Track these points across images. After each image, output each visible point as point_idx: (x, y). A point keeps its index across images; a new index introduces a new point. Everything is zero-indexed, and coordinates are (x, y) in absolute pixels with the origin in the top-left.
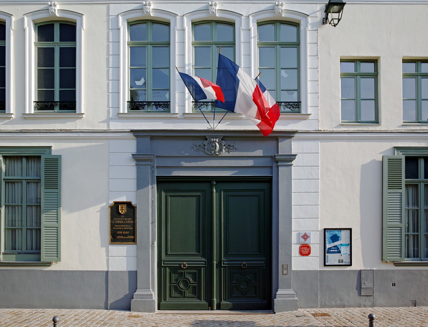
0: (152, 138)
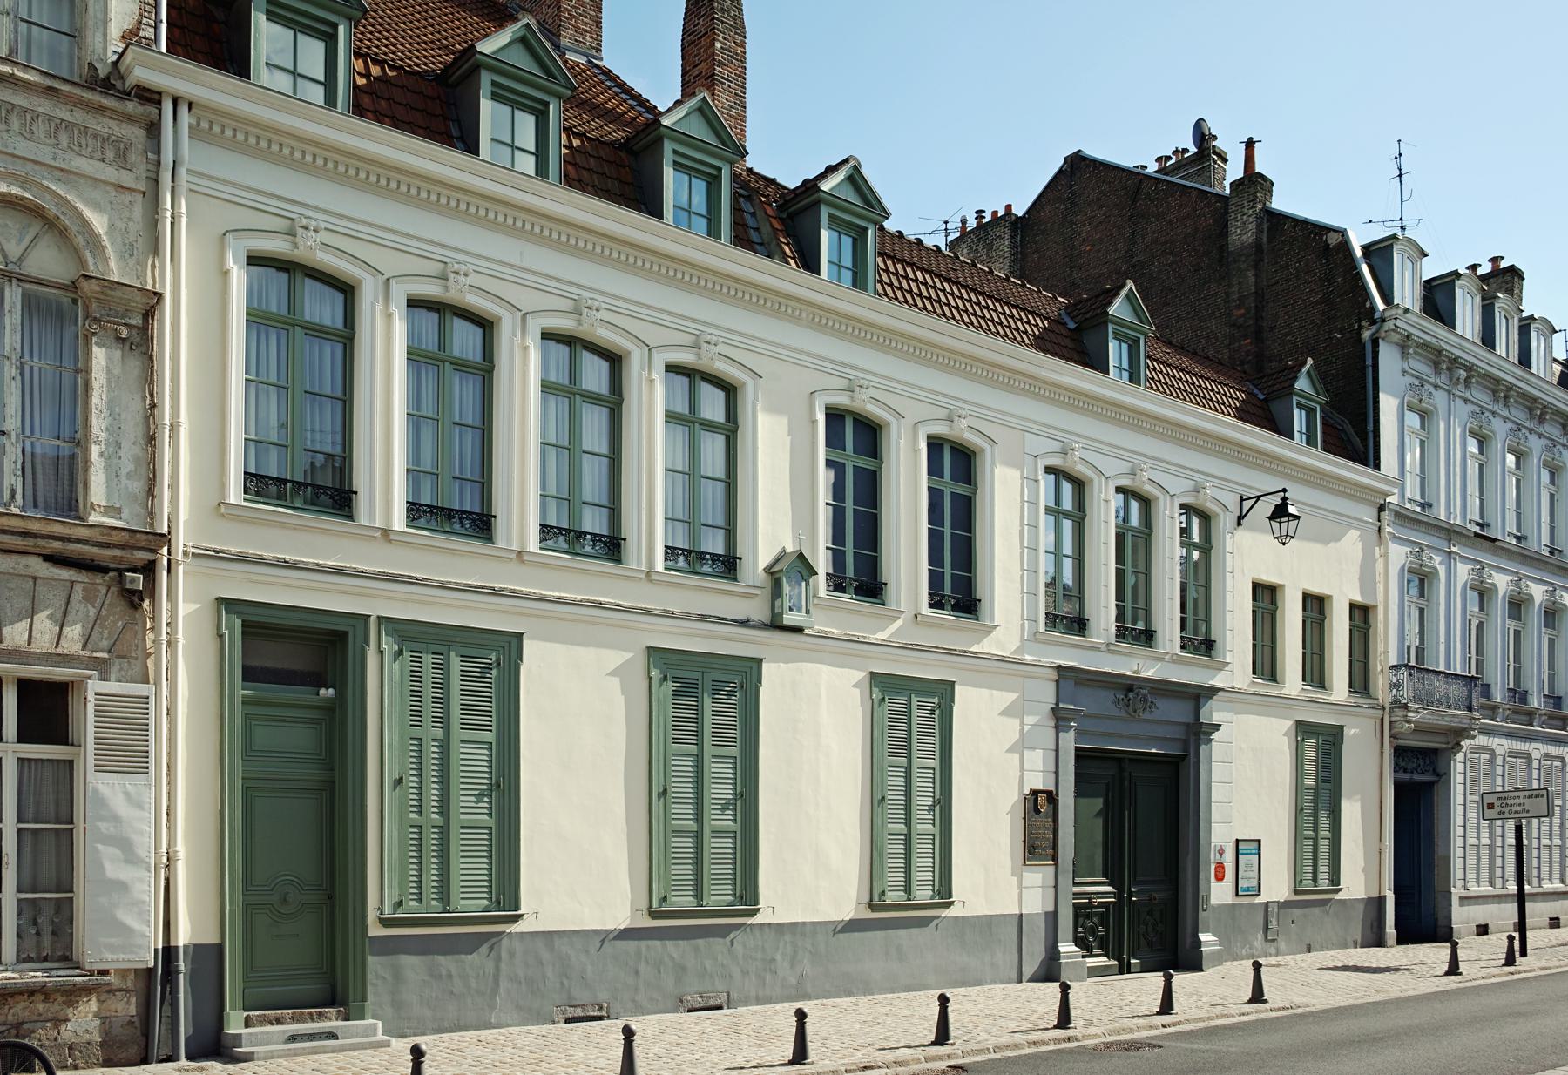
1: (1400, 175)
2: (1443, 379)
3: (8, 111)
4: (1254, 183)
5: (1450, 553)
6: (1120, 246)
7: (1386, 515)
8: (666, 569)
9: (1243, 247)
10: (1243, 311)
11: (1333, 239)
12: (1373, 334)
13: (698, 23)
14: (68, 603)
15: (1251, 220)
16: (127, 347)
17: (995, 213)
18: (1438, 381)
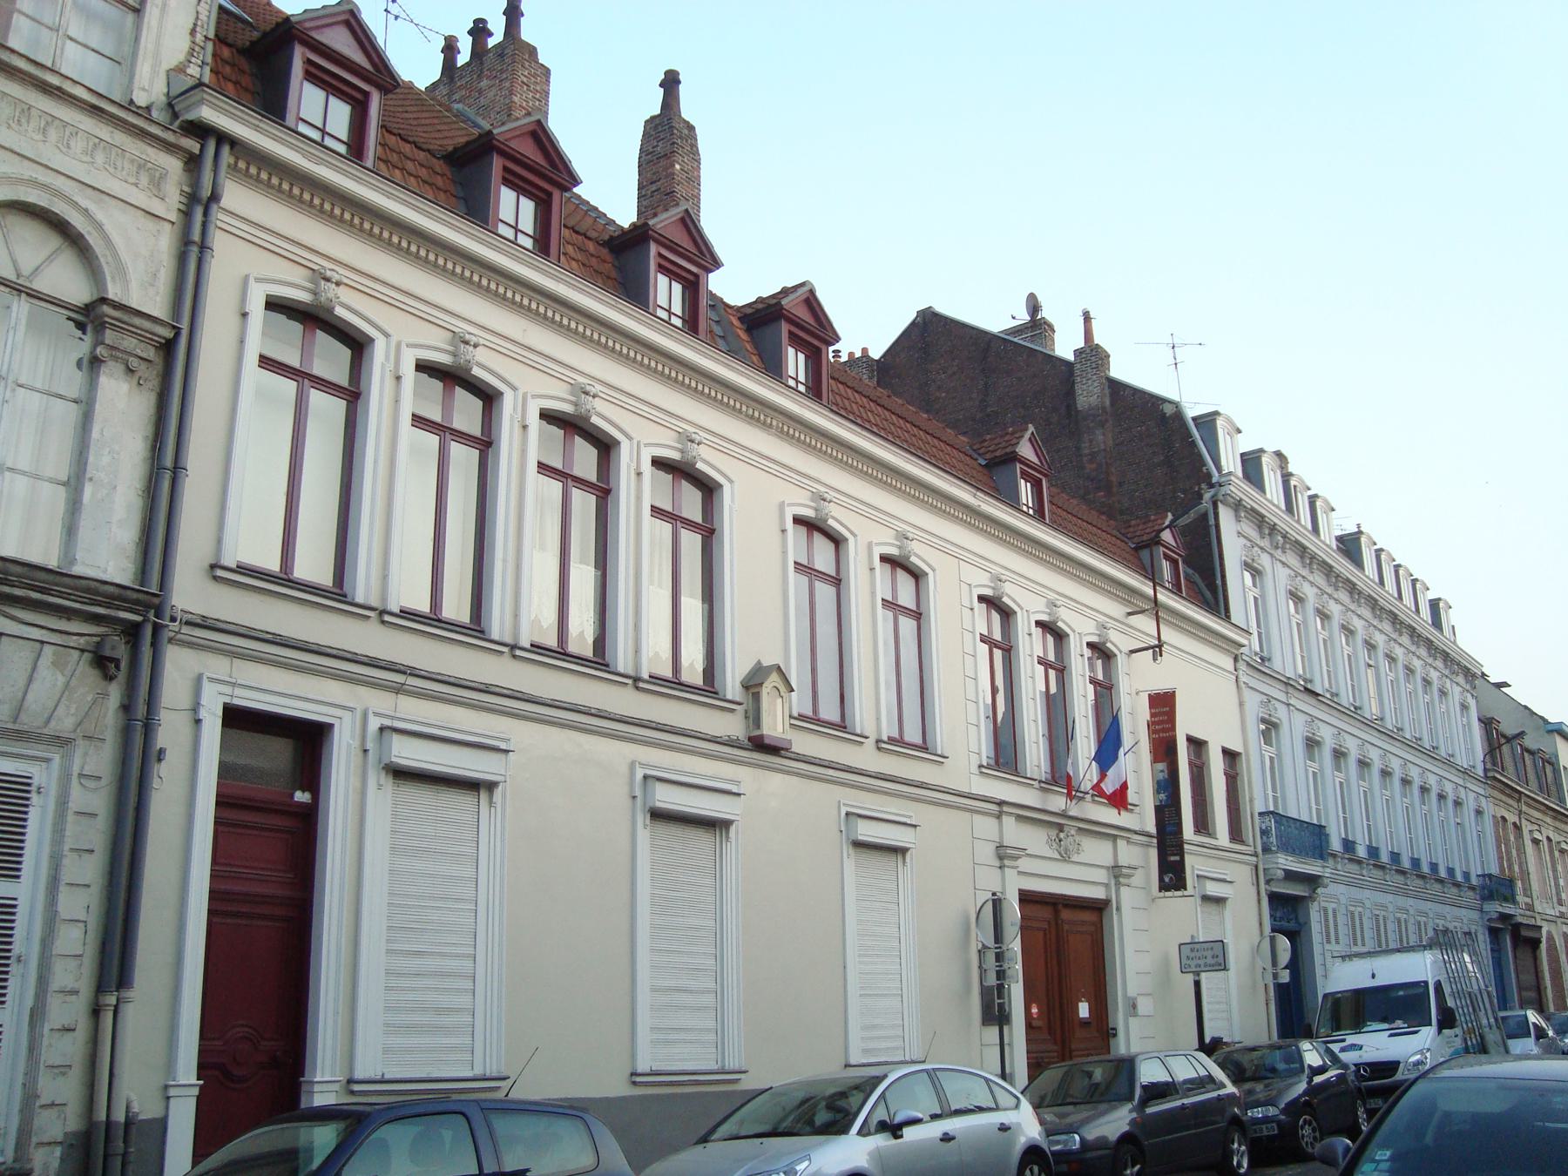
0: (1019, 818)
1: (1176, 364)
2: (1265, 543)
3: (47, 123)
4: (1093, 355)
5: (1288, 705)
6: (974, 395)
7: (1242, 666)
8: (650, 677)
9: (1091, 408)
10: (1094, 466)
11: (1168, 409)
12: (1213, 497)
13: (657, 146)
14: (34, 668)
15: (1096, 384)
16: (135, 381)
17: (851, 354)
18: (1262, 545)
